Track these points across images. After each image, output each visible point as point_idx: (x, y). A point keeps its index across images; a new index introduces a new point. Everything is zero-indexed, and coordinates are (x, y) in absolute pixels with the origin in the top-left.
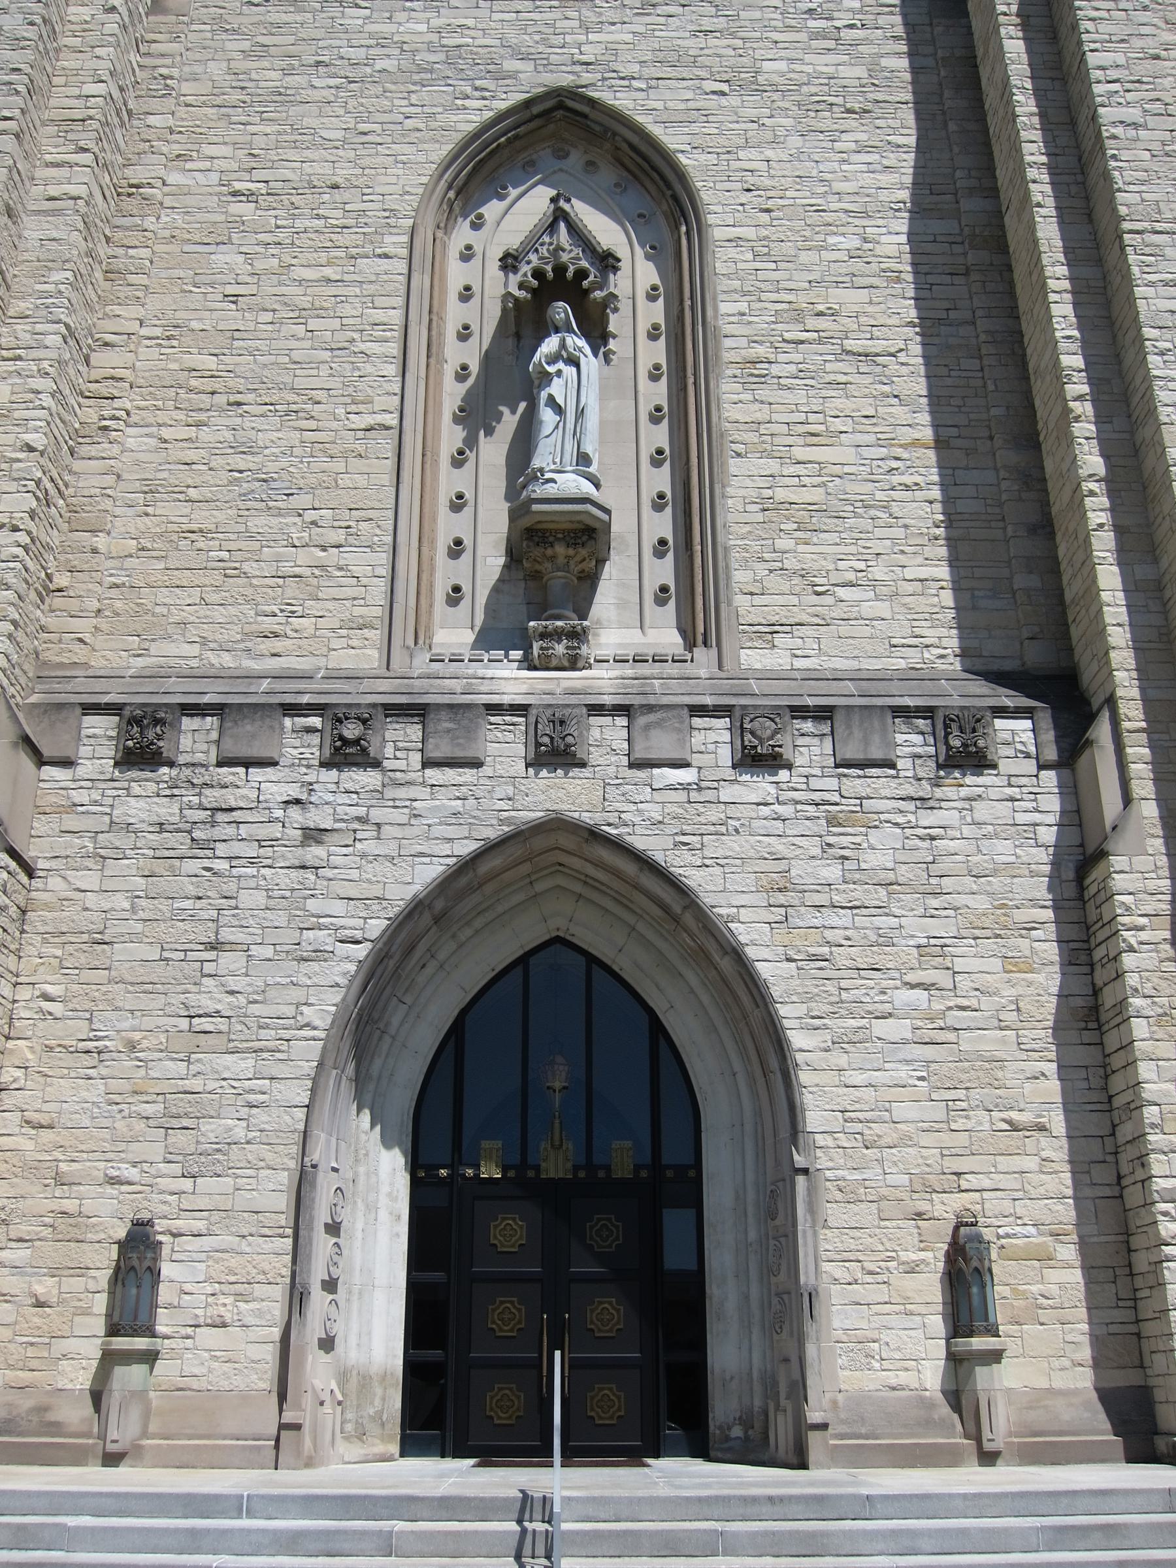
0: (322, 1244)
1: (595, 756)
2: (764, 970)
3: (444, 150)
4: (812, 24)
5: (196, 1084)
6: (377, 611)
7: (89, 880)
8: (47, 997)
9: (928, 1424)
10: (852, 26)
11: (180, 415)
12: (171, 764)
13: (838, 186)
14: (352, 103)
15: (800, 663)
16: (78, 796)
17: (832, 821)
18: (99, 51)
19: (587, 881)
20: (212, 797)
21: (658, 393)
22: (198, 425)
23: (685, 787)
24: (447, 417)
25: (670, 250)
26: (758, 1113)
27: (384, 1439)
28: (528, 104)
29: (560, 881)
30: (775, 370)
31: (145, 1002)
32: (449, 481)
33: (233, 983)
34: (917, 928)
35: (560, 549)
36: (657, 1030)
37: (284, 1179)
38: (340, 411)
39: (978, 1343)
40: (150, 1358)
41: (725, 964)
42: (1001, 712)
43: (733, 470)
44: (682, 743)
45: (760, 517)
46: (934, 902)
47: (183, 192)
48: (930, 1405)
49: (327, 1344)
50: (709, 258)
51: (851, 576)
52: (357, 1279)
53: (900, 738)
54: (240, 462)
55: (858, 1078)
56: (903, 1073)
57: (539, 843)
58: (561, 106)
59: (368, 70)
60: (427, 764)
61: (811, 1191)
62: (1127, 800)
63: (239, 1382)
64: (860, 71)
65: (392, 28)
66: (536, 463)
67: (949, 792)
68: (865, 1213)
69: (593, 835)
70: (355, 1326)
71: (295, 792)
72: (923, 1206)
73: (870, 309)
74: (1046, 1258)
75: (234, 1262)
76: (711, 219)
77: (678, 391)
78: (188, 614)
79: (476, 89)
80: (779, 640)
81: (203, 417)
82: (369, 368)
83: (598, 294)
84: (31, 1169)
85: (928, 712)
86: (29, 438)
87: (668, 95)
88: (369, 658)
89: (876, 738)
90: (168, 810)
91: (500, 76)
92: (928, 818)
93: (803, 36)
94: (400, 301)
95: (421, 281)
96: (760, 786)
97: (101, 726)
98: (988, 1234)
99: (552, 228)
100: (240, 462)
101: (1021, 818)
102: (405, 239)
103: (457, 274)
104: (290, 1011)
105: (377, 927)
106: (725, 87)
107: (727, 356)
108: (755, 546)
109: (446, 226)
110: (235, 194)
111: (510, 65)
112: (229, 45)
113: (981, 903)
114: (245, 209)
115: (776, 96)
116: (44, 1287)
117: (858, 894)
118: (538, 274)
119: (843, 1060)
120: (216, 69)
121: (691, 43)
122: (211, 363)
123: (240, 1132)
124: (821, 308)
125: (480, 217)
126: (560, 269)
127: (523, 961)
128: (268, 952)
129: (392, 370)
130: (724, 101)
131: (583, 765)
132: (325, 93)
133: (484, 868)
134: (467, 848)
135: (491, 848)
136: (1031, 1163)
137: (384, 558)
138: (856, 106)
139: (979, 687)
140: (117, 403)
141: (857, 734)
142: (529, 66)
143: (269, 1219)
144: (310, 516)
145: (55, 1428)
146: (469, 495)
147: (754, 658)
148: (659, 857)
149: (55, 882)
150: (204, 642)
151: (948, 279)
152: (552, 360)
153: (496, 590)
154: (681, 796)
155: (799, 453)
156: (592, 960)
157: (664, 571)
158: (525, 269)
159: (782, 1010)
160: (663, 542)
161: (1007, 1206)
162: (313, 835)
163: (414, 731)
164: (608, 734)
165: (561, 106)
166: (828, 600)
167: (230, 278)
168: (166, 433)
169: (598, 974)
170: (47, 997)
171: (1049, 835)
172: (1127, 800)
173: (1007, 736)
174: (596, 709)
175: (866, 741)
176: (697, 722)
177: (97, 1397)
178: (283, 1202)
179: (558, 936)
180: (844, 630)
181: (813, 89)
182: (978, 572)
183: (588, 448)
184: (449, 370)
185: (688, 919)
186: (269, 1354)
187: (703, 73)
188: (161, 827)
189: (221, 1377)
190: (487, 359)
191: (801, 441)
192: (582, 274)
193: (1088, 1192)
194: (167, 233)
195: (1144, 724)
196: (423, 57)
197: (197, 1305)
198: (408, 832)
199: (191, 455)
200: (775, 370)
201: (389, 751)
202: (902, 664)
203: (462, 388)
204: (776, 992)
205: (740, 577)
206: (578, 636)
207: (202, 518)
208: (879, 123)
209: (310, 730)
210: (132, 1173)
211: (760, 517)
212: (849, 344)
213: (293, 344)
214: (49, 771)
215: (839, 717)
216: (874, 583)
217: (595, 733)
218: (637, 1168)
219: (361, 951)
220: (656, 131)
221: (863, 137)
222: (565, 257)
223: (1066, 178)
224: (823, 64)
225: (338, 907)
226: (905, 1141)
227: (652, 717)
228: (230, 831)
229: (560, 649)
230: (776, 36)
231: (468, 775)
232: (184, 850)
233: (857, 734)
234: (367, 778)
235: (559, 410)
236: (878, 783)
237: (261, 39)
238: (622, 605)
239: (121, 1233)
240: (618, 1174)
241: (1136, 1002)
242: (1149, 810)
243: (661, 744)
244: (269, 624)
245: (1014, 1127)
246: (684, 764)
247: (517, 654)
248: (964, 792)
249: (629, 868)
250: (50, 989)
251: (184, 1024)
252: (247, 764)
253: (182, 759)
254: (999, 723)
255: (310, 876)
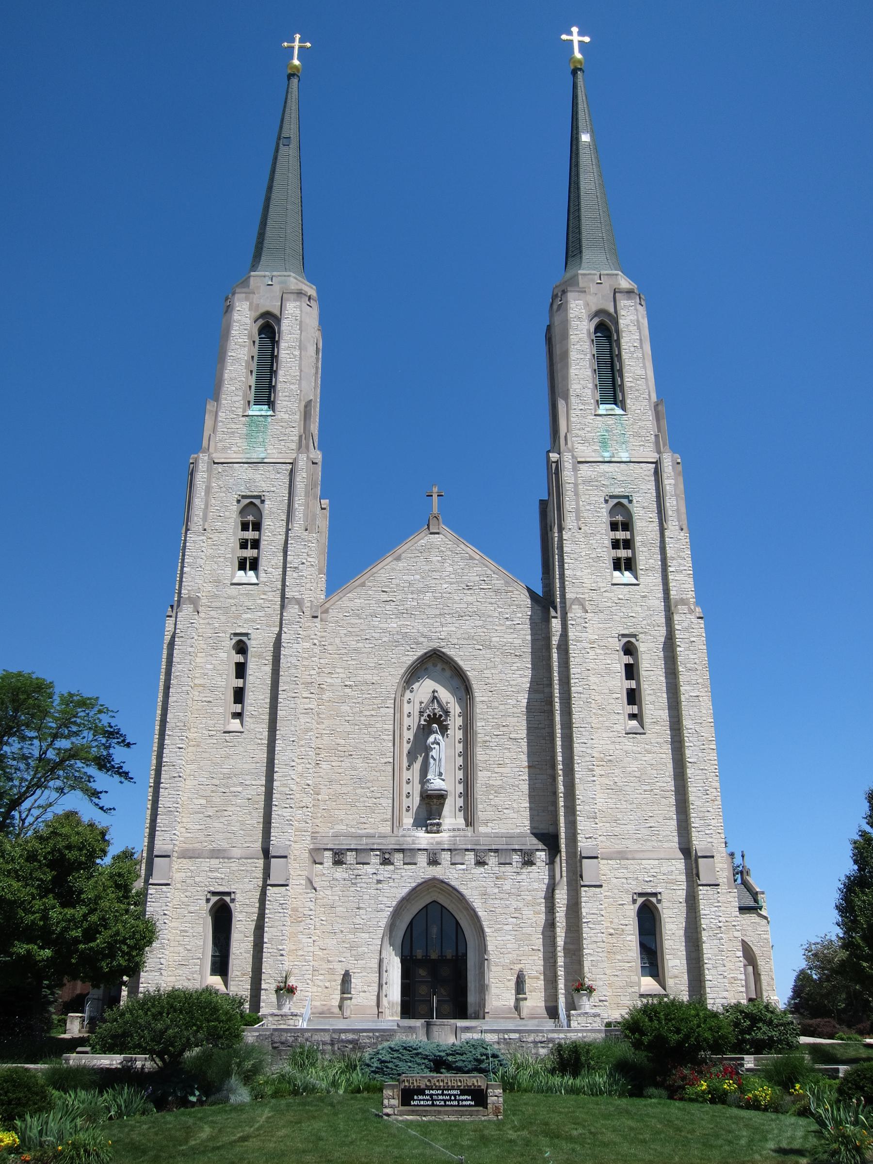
0: (385, 974)
1: (443, 862)
2: (480, 914)
3: (403, 671)
4: (508, 623)
5: (356, 940)
6: (389, 817)
7: (329, 892)
8: (322, 920)
9: (510, 1013)
10: (518, 624)
11: (336, 758)
12: (345, 864)
13: (512, 683)
14: (377, 653)
15: (493, 831)
16: (325, 872)
17: (497, 878)
18: (313, 659)
19: (441, 889)
20: (356, 872)
21: (460, 747)
22: (341, 761)
23: (464, 870)
24: (405, 755)
25: (465, 701)
26: (479, 945)
27: (397, 1017)
28: (426, 654)
29: (435, 889)
30: (491, 744)
31: (344, 921)
32: (406, 775)
33: (363, 917)
34: (515, 904)
35: (435, 800)
36: (457, 923)
37: (376, 961)
38: (378, 757)
39: (521, 996)
40: (351, 999)
41: (472, 912)
42: (538, 850)
43: (479, 775)
44: (463, 858)
45: (485, 789)
46: (519, 898)
47: (332, 685)
48: (512, 1009)
49: (386, 996)
50: (475, 709)
51: (507, 806)
52: (391, 982)
53: (514, 857)
54: (353, 773)
55: (499, 938)
56: (509, 937)
57: (430, 882)
58: (435, 653)
59: (380, 641)
60: (404, 864)
61: (488, 964)
62: (561, 876)
63: (369, 1004)
64: (520, 641)
65: (387, 625)
66: (429, 777)
67: (524, 870)
68: (500, 968)
69: (442, 882)
70: (391, 993)
71: (374, 871)
72: (512, 967)
73: (518, 724)
74: (538, 978)
75: (366, 979)
76: (476, 694)
77: (466, 748)
78: (343, 817)
79: (411, 648)
80: (489, 824)
81: (342, 759)
82: (385, 744)
83: (445, 723)
84: (322, 959)
85: (520, 850)
86: (308, 782)
87: (465, 650)
88: (386, 829)
89: (508, 858)
90: (346, 876)
91: (417, 643)
92: (519, 877)
93: (504, 628)
94: (392, 722)
95: (397, 716)
96: (481, 869)
97: (328, 854)
98: (525, 973)
99: (433, 701)
100: (353, 773)
101: (540, 877)
102: (393, 701)
103: (407, 708)
104: (376, 923)
105: (394, 904)
106: (481, 647)
107: (479, 740)
108: (484, 798)
109: (405, 689)
110: (346, 686)
111: (421, 639)
112: (341, 632)
113: (530, 898)
114: (348, 690)
115: (495, 650)
116: (327, 984)
117: (502, 895)
118: (429, 716)
119: (496, 935)
120: (337, 641)
121: (472, 631)
122: (343, 742)
123: (366, 951)
124: (504, 724)
125: (413, 688)
126: (435, 714)
127: (426, 906)
128: (370, 910)
129: (391, 744)
130: (481, 652)
131: (440, 864)
132: (369, 649)
133: (418, 889)
134: (414, 885)
135: (419, 885)
136: (536, 958)
137: (391, 801)
138: (518, 654)
139: (535, 841)
140: (320, 756)
141: (504, 856)
142: (426, 640)
143: (373, 969)
144: (372, 789)
145: (332, 1013)
146: (411, 779)
147: (482, 829)
148: (457, 887)
149: (321, 893)
150: (347, 825)
151: (539, 714)
152: (433, 744)
153: (418, 807)
154: (462, 872)
155: (497, 770)
156: (442, 906)
157: (460, 802)
158: (426, 715)
159: (484, 923)
160: (461, 793)
161: (531, 967)
162: (379, 882)
163: (401, 855)
164: (446, 856)
165: (435, 653)
166: (502, 813)
167: (346, 715)
168: (333, 764)
169: (444, 910)
170: (322, 920)
171: (546, 881)
172: (561, 876)
173: (538, 856)
174: (443, 850)
175: (506, 858)
176: (467, 853)
177: (340, 1007)
178: (376, 966)
179: (434, 879)
180: (505, 821)
181: (506, 648)
182: (540, 805)
183: (442, 771)
184: (405, 740)
185: (463, 901)
186: (375, 998)
187: (475, 642)
188: (345, 880)
189: (366, 1003)
190: (415, 736)
191: (496, 766)
192: (441, 716)
193: (548, 964)
194: (328, 699)
195: (712, 720)
196: (396, 637)
197: (359, 988)
198: (401, 881)
199: (340, 771)
200: (491, 744)
201: (396, 861)
202: (519, 831)
203: (410, 745)
204: (482, 919)
205: (480, 806)
206: (439, 825)
207: (345, 790)
208: (524, 660)
209: (377, 855)
210: (344, 960)
211: (485, 789)
212: (512, 736)
213: (365, 736)
214: (318, 866)
215: (500, 852)
216: (513, 808)
217: (443, 856)
218: (453, 956)
219: (391, 909)
220: (461, 663)
221: (519, 665)
222: (436, 711)
223: (565, 701)
224: (509, 638)
225: (385, 899)
226: (509, 953)
227: (456, 852)
228: (360, 880)
229: (435, 828)
230: (496, 628)
231: (414, 867)
232: (350, 885)
233: (504, 856)
234: (391, 867)
235: (435, 760)
236: (508, 868)
237: (349, 629)
238: (450, 811)
239: (343, 973)
240: (448, 958)
241: (558, 924)
242: (565, 879)
243: (458, 859)
244: (362, 820)
245: (533, 950)
246: (463, 864)
247: (424, 829)
248: (528, 871)
249: (451, 889)
250: (323, 919)
251: (353, 926)
252: (363, 864)
253: (348, 863)
254: (537, 853)
255: (378, 891)
